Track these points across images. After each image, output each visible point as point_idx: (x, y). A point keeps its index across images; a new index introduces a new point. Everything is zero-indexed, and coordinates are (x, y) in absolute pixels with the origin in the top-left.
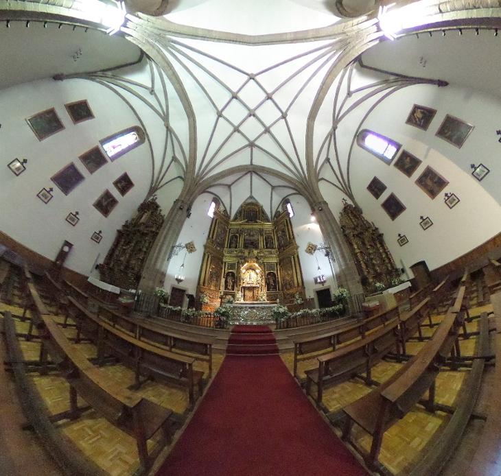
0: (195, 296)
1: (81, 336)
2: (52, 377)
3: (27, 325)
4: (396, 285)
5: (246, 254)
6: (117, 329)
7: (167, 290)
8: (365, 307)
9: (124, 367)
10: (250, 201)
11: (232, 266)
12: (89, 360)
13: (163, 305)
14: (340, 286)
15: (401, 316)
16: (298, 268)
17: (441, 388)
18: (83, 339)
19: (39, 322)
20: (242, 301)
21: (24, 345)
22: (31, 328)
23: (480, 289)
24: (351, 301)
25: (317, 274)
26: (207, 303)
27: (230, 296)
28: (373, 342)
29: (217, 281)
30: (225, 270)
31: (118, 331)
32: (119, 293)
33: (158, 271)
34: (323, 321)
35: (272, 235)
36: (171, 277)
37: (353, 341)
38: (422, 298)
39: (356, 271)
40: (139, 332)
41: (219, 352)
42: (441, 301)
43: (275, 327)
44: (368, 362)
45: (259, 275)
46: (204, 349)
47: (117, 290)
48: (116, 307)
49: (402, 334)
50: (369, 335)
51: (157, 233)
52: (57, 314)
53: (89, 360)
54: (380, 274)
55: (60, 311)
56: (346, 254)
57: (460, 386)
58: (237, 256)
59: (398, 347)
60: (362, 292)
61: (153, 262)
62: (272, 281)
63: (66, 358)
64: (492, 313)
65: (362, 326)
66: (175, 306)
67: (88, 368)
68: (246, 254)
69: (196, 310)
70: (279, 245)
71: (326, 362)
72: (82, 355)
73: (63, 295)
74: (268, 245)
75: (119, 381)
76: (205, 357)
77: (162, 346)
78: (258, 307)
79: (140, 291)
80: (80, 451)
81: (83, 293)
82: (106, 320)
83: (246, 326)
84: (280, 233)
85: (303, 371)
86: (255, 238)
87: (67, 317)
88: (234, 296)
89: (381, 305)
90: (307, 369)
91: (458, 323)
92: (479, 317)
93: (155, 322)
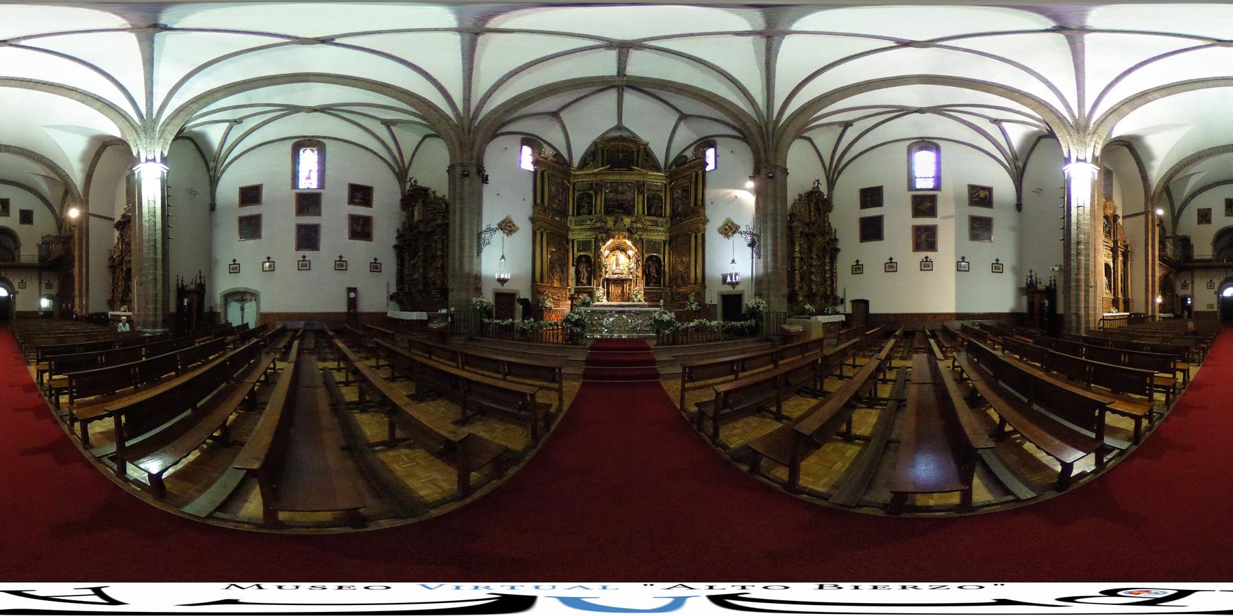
0: (530, 300)
1: (396, 374)
2: (371, 414)
3: (343, 374)
4: (828, 314)
5: (610, 224)
6: (435, 361)
7: (488, 298)
8: (785, 330)
9: (447, 402)
10: (618, 134)
11: (585, 245)
12: (407, 396)
13: (486, 320)
14: (758, 294)
15: (824, 349)
16: (700, 249)
17: (858, 421)
18: (398, 377)
19: (353, 369)
20: (605, 302)
21: (344, 390)
22: (347, 375)
23: (907, 346)
24: (768, 318)
25: (729, 269)
26: (550, 308)
27: (585, 295)
28: (787, 373)
29: (562, 271)
30: (574, 253)
31: (436, 363)
32: (426, 318)
33: (469, 275)
34: (725, 339)
35: (663, 195)
36: (490, 279)
37: (762, 369)
38: (851, 336)
39: (786, 280)
40: (462, 361)
41: (572, 377)
42: (869, 346)
43: (654, 342)
44: (778, 395)
45: (633, 260)
46: (551, 375)
47: (423, 316)
48: (428, 336)
49: (826, 368)
50: (783, 365)
52: (367, 359)
53: (407, 396)
54: (815, 295)
55: (370, 355)
56: (779, 254)
57: (875, 420)
58: (591, 229)
59: (815, 382)
60: (785, 310)
61: (457, 266)
62: (653, 270)
63: (384, 397)
64: (911, 367)
65: (777, 352)
66: (503, 319)
67: (407, 405)
68: (610, 224)
69: (535, 320)
70: (673, 211)
71: (724, 392)
72: (399, 393)
73: (368, 339)
74: (653, 211)
75: (442, 415)
76: (553, 385)
77: (494, 375)
78: (630, 312)
79: (453, 309)
80: (392, 471)
81: (387, 331)
82: (420, 353)
83: (612, 340)
84: (678, 193)
85: (694, 402)
86: (628, 196)
87: (378, 359)
88: (591, 294)
89: (804, 331)
90: (699, 401)
91: (879, 369)
92: (899, 368)
93: (479, 345)
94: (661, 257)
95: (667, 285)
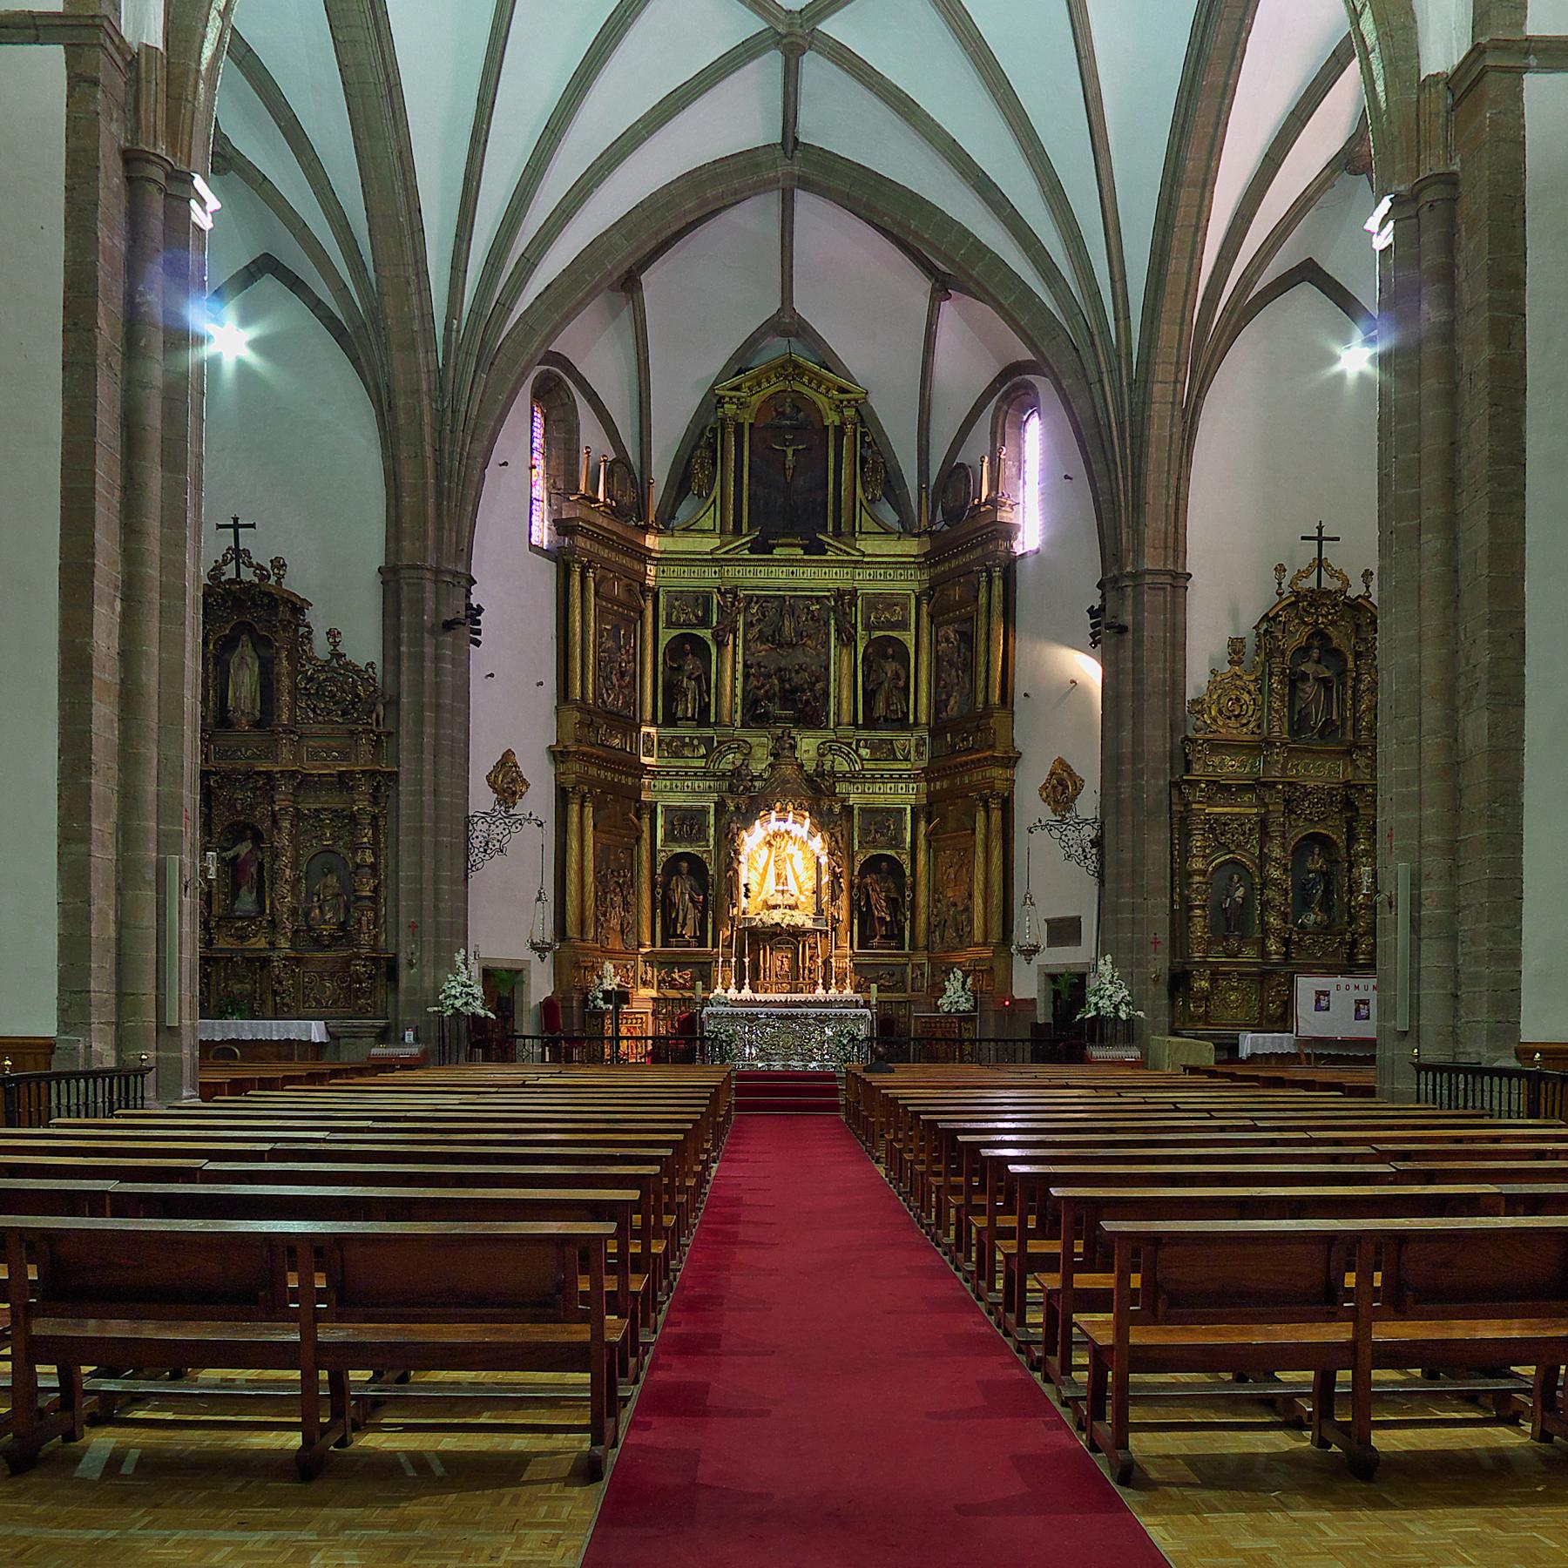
11: (686, 823)
51: (384, 783)
70: (938, 705)
74: (880, 709)
94: (905, 859)
95: (922, 941)
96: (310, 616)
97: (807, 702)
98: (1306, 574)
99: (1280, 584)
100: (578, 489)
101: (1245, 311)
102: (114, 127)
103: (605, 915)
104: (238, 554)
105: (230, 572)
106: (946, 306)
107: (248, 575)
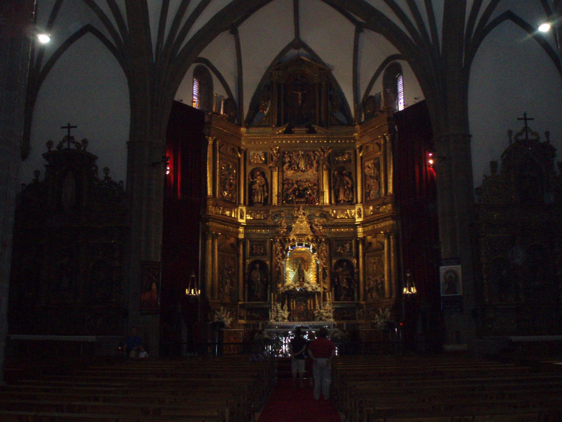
74: (342, 197)
96: (98, 163)
97: (310, 195)
98: (520, 134)
99: (510, 138)
100: (212, 109)
101: (483, 32)
102: (290, 150)
103: (222, 287)
104: (69, 138)
105: (65, 145)
106: (362, 35)
107: (72, 146)
